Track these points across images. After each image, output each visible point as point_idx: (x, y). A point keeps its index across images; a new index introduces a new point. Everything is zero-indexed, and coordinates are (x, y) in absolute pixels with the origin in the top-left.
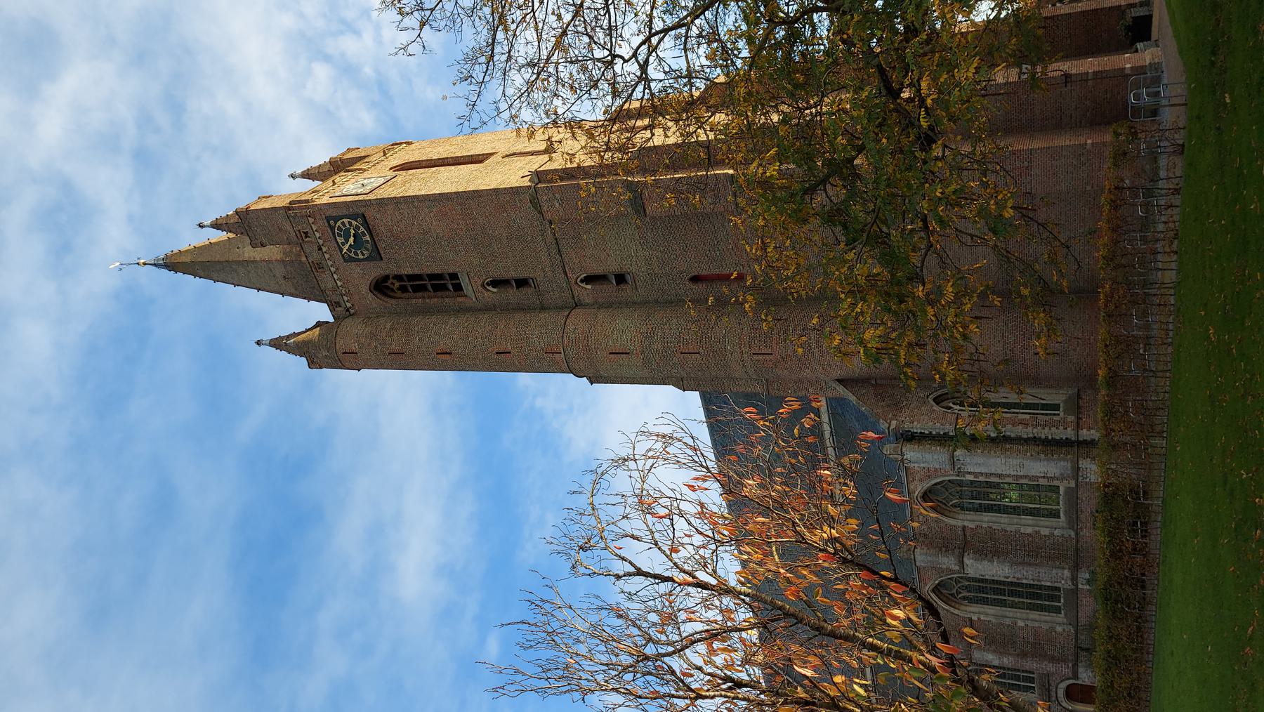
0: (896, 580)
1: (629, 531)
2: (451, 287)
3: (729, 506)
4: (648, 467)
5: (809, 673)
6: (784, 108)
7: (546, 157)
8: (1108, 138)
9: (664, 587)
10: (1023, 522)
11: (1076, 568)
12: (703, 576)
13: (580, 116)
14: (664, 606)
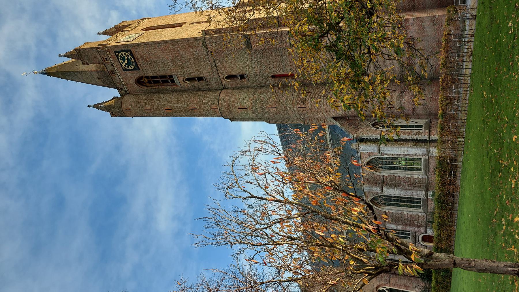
0: (356, 196)
5: (321, 234)
8: (445, 13)
9: (263, 202)
10: (407, 173)
11: (427, 190)
12: (278, 197)
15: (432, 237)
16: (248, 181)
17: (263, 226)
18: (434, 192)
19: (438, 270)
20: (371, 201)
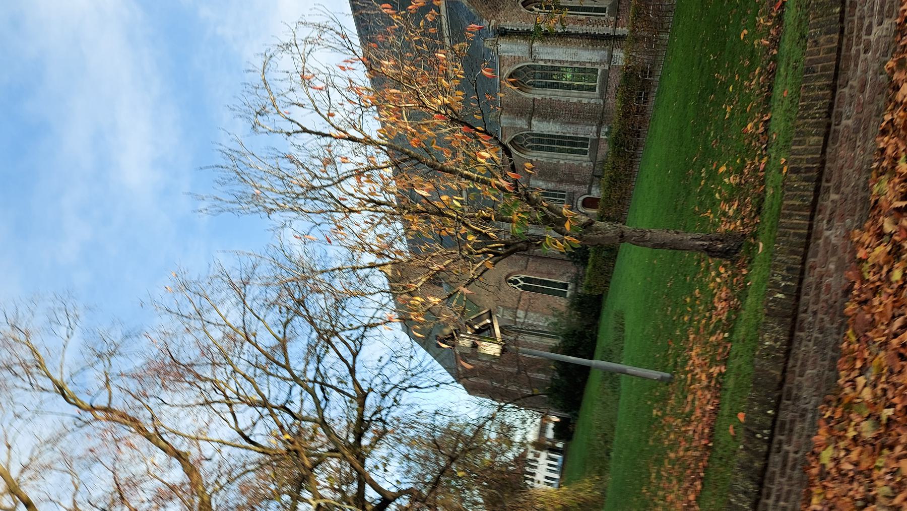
0: (485, 132)
5: (425, 193)
9: (325, 141)
10: (572, 94)
11: (600, 125)
12: (352, 132)
15: (598, 200)
16: (296, 102)
17: (325, 183)
18: (610, 128)
19: (599, 247)
20: (510, 143)
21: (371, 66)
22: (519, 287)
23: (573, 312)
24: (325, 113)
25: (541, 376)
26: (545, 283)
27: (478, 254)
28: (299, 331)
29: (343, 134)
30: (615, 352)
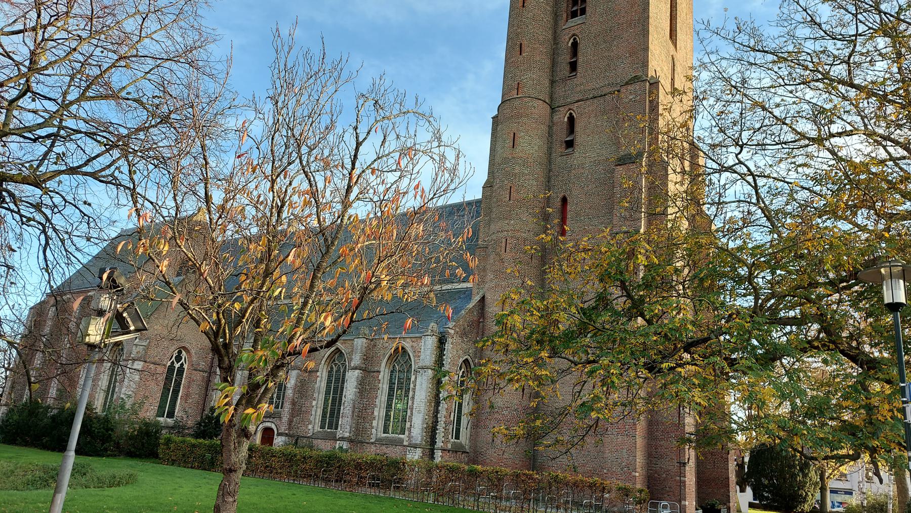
0: (352, 321)
1: (388, 139)
2: (574, 9)
3: (405, 214)
4: (434, 156)
5: (291, 258)
6: (686, 271)
7: (669, 89)
8: (639, 486)
9: (348, 163)
10: (382, 410)
11: (350, 440)
12: (355, 191)
13: (699, 117)
14: (334, 161)
18: (347, 451)
19: (218, 451)
21: (418, 214)
22: (173, 363)
23: (137, 426)
24: (375, 165)
25: (53, 392)
26: (176, 392)
27: (218, 314)
28: (130, 115)
29: (355, 180)
30: (83, 479)
